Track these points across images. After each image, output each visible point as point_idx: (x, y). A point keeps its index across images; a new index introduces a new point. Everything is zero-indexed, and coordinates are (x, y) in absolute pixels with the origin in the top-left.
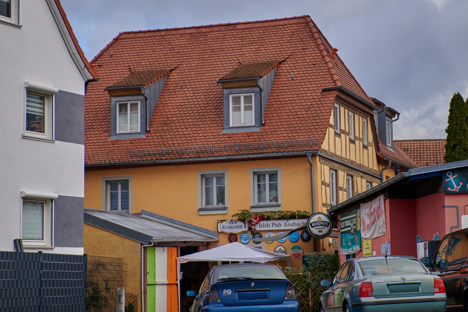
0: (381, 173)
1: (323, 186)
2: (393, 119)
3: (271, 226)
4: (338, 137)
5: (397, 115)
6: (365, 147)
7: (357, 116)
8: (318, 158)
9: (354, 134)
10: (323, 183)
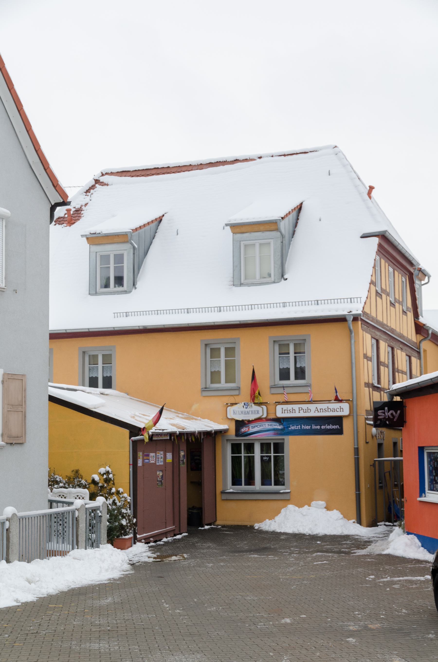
0: (419, 345)
1: (365, 360)
2: (423, 282)
3: (297, 411)
4: (379, 297)
5: (427, 278)
6: (404, 312)
7: (396, 273)
8: (360, 322)
9: (395, 295)
10: (365, 356)
